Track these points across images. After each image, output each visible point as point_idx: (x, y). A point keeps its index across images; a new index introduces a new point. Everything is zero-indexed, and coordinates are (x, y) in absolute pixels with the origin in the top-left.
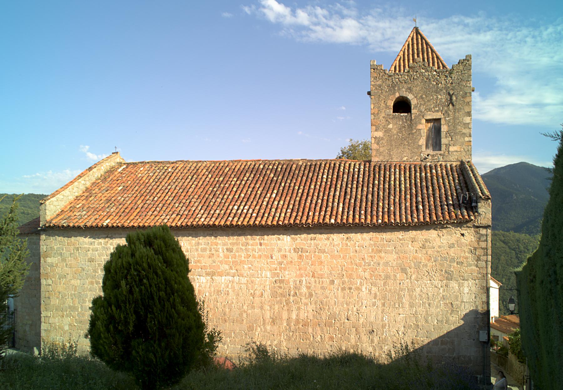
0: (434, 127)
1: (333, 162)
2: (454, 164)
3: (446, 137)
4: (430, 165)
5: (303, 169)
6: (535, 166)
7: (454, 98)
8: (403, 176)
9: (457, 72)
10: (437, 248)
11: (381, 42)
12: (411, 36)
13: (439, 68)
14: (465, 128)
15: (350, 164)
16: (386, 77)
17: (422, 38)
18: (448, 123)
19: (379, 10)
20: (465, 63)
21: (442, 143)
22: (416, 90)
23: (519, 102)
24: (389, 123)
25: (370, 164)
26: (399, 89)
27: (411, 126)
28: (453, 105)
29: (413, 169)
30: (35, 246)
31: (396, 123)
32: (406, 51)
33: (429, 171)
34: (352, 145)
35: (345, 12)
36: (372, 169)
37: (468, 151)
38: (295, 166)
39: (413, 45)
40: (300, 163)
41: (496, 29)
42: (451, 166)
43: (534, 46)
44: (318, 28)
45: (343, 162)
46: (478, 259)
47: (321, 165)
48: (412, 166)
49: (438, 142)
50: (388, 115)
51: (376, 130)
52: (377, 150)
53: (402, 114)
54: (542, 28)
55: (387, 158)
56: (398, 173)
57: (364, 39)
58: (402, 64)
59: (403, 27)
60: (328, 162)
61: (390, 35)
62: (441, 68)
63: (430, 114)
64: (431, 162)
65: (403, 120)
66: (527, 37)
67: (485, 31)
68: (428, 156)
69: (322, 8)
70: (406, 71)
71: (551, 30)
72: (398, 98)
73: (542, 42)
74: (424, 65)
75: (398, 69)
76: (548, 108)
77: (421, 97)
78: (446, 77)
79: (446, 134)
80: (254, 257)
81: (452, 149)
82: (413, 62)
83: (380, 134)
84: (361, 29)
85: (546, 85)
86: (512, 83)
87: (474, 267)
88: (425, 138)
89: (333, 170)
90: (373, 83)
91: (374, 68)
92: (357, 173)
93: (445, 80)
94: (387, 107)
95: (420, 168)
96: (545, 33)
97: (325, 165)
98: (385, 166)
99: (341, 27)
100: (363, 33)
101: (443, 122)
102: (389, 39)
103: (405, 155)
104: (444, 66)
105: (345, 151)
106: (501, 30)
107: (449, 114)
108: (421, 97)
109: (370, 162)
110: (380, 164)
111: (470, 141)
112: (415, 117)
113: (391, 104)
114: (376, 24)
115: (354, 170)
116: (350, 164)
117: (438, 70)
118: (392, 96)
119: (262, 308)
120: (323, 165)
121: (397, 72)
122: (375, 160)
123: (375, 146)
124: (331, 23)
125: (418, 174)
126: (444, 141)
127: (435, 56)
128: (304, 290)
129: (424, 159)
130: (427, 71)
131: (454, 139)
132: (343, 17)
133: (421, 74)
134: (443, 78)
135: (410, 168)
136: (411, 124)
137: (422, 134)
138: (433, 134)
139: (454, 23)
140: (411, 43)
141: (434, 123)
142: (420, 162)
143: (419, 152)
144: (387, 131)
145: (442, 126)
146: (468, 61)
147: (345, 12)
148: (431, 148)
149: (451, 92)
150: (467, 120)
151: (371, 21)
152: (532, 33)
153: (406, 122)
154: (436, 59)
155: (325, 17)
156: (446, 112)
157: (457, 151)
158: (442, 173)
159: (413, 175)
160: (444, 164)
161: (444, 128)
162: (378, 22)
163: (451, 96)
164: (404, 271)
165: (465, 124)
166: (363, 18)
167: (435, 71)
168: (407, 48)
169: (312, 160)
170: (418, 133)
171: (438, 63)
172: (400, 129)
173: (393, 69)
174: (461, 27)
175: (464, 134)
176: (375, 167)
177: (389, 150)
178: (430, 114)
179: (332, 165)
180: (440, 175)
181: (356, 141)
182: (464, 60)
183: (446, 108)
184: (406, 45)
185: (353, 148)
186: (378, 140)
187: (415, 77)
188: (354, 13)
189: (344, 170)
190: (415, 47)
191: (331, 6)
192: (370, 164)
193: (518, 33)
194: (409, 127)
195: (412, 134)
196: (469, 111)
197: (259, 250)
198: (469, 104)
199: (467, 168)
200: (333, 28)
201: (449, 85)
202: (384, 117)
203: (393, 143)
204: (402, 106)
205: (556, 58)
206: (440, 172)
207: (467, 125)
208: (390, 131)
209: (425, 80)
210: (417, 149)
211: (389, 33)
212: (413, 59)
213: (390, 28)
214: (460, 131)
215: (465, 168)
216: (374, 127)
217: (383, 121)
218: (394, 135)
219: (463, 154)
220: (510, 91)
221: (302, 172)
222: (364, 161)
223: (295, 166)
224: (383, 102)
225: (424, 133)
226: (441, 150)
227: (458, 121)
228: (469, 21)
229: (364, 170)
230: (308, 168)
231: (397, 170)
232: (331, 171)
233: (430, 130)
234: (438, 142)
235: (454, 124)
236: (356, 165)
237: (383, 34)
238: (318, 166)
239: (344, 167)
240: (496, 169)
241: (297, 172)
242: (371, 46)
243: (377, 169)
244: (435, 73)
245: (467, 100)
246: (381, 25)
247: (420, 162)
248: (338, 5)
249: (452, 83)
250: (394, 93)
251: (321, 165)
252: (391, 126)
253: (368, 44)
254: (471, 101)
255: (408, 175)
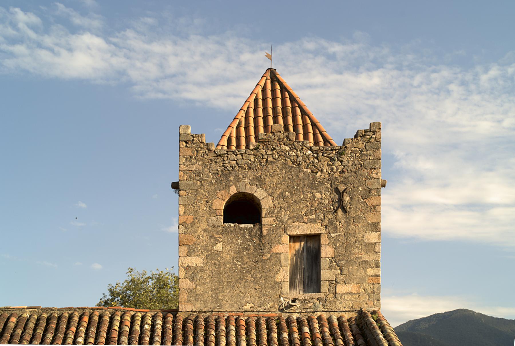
0: (308, 249)
1: (97, 313)
2: (346, 316)
3: (330, 268)
4: (298, 319)
5: (32, 325)
6: (485, 316)
7: (346, 198)
8: (244, 338)
9: (353, 152)
11: (157, 80)
12: (262, 84)
13: (316, 143)
14: (367, 252)
15: (133, 317)
16: (211, 156)
17: (284, 89)
18: (334, 243)
19: (150, 21)
20: (370, 137)
21: (322, 279)
22: (271, 182)
23: (441, 200)
24: (216, 241)
25: (175, 317)
26: (237, 180)
27: (260, 248)
28: (345, 211)
29: (265, 326)
31: (230, 243)
32: (252, 111)
33: (295, 329)
34: (133, 281)
35: (77, 20)
36: (180, 326)
37: (373, 292)
38: (14, 320)
39: (264, 100)
40: (27, 315)
41: (389, 66)
42: (339, 319)
43: (465, 99)
44: (20, 49)
45: (119, 313)
47: (71, 317)
48: (263, 321)
49: (314, 277)
50: (214, 226)
51: (189, 254)
52: (190, 291)
53: (242, 226)
54: (479, 69)
55: (210, 306)
56: (233, 333)
57: (122, 73)
58: (243, 134)
59: (203, 55)
60: (87, 312)
61: (219, 82)
62: (322, 144)
63: (298, 227)
64: (300, 313)
65: (244, 235)
66: (450, 82)
67: (369, 70)
68: (294, 301)
69: (25, 10)
70: (251, 147)
71: (494, 72)
72: (235, 195)
73: (480, 93)
74: (287, 137)
75: (234, 144)
76: (496, 212)
77: (282, 195)
78: (332, 159)
79: (331, 262)
81: (341, 289)
82: (266, 131)
83: (196, 261)
84: (114, 54)
85: (490, 170)
86: (425, 165)
88: (287, 269)
89: (98, 328)
90: (183, 167)
91: (187, 140)
92: (148, 333)
93: (328, 165)
94: (212, 211)
95: (279, 324)
96: (484, 78)
97: (80, 318)
98: (206, 320)
99: (70, 50)
100: (118, 62)
101: (324, 240)
102: (173, 76)
103: (248, 299)
104: (326, 141)
105: (118, 290)
106: (399, 68)
107: (336, 227)
108: (282, 195)
109: (175, 312)
110: (197, 317)
111: (378, 276)
112: (269, 230)
113: (220, 205)
114: (147, 47)
115: (142, 327)
116: (133, 317)
117: (314, 148)
118: (223, 192)
120: (76, 319)
121: (234, 148)
122: (186, 308)
123: (185, 283)
124: (48, 40)
125: (275, 335)
126: (326, 274)
127: (309, 122)
129: (287, 308)
130: (293, 148)
131: (345, 272)
132: (75, 30)
133: (283, 154)
134: (325, 161)
135: (258, 324)
136: (261, 244)
137: (283, 263)
138: (304, 262)
139: (308, 51)
140: (260, 96)
141: (306, 243)
142: (278, 314)
143: (279, 293)
144: (211, 256)
145: (322, 248)
146: (374, 132)
147: (77, 20)
148: (301, 287)
149: (341, 188)
150: (372, 237)
151: (134, 41)
152: (460, 76)
153: (251, 240)
154: (310, 127)
155: (33, 28)
156: (331, 222)
157: (351, 293)
158: (322, 332)
159: (265, 336)
160: (325, 316)
161: (327, 252)
162: (150, 41)
163: (340, 194)
165: (366, 245)
166: (117, 34)
167: (311, 149)
168: (252, 105)
169: (52, 310)
170: (274, 259)
171: (315, 135)
172: (239, 252)
173: (225, 142)
174: (320, 59)
175: (366, 262)
176: (185, 321)
177: (216, 291)
178: (298, 227)
179: (96, 318)
180: (319, 336)
181: (141, 272)
182: (366, 131)
183: (330, 216)
184: (252, 101)
185: (135, 285)
186: (192, 273)
187: (270, 159)
188: (96, 23)
189: (120, 327)
190: (270, 104)
191: (43, 8)
192: (175, 317)
193: (434, 76)
194: (255, 250)
195: (263, 261)
196: (375, 221)
198: (375, 209)
199: (371, 324)
200: (52, 50)
201: (337, 175)
202: (205, 230)
203: (224, 278)
204: (243, 210)
205: (507, 123)
206: (317, 331)
207: (371, 247)
208: (219, 255)
209: (291, 164)
210: (273, 288)
211: (173, 64)
212: (266, 126)
213: (176, 55)
214: (359, 257)
215: (368, 324)
216: (185, 249)
217: (205, 237)
218: (225, 264)
219: (363, 299)
220: (420, 179)
221: (31, 332)
222: (163, 311)
223: (14, 320)
224: (204, 202)
225: (286, 259)
226: (319, 291)
227: (353, 239)
228: (336, 48)
229: (163, 327)
230: (43, 323)
231: (233, 328)
232: (93, 329)
233: (298, 255)
234: (314, 277)
235: (347, 243)
236: (146, 317)
237: (161, 66)
238: (65, 321)
239: (121, 323)
240: (410, 321)
241: (19, 331)
242: (137, 88)
243: (190, 326)
244: (309, 152)
245: (372, 201)
246: (156, 48)
247: (278, 314)
248: (61, 6)
249: (342, 172)
250: (227, 187)
251: (71, 317)
252: (219, 247)
253: (131, 84)
254: (379, 205)
255: (254, 336)
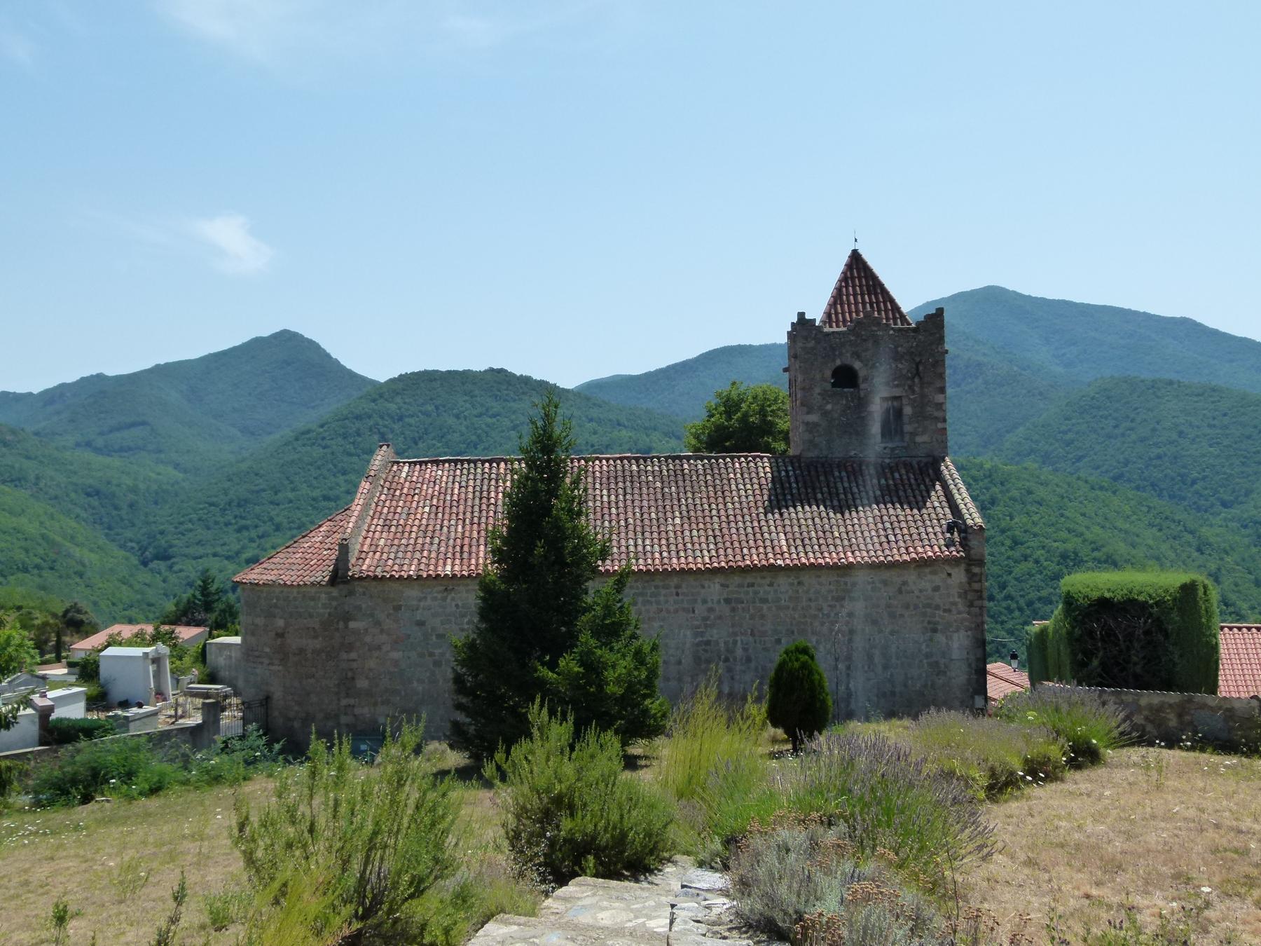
7: (921, 368)
10: (917, 593)
28: (921, 378)
30: (312, 603)
46: (971, 605)
51: (808, 413)
80: (668, 611)
87: (966, 615)
101: (905, 401)
119: (680, 680)
128: (739, 652)
144: (825, 414)
164: (875, 622)
197: (675, 602)
216: (805, 409)
250: (834, 360)
